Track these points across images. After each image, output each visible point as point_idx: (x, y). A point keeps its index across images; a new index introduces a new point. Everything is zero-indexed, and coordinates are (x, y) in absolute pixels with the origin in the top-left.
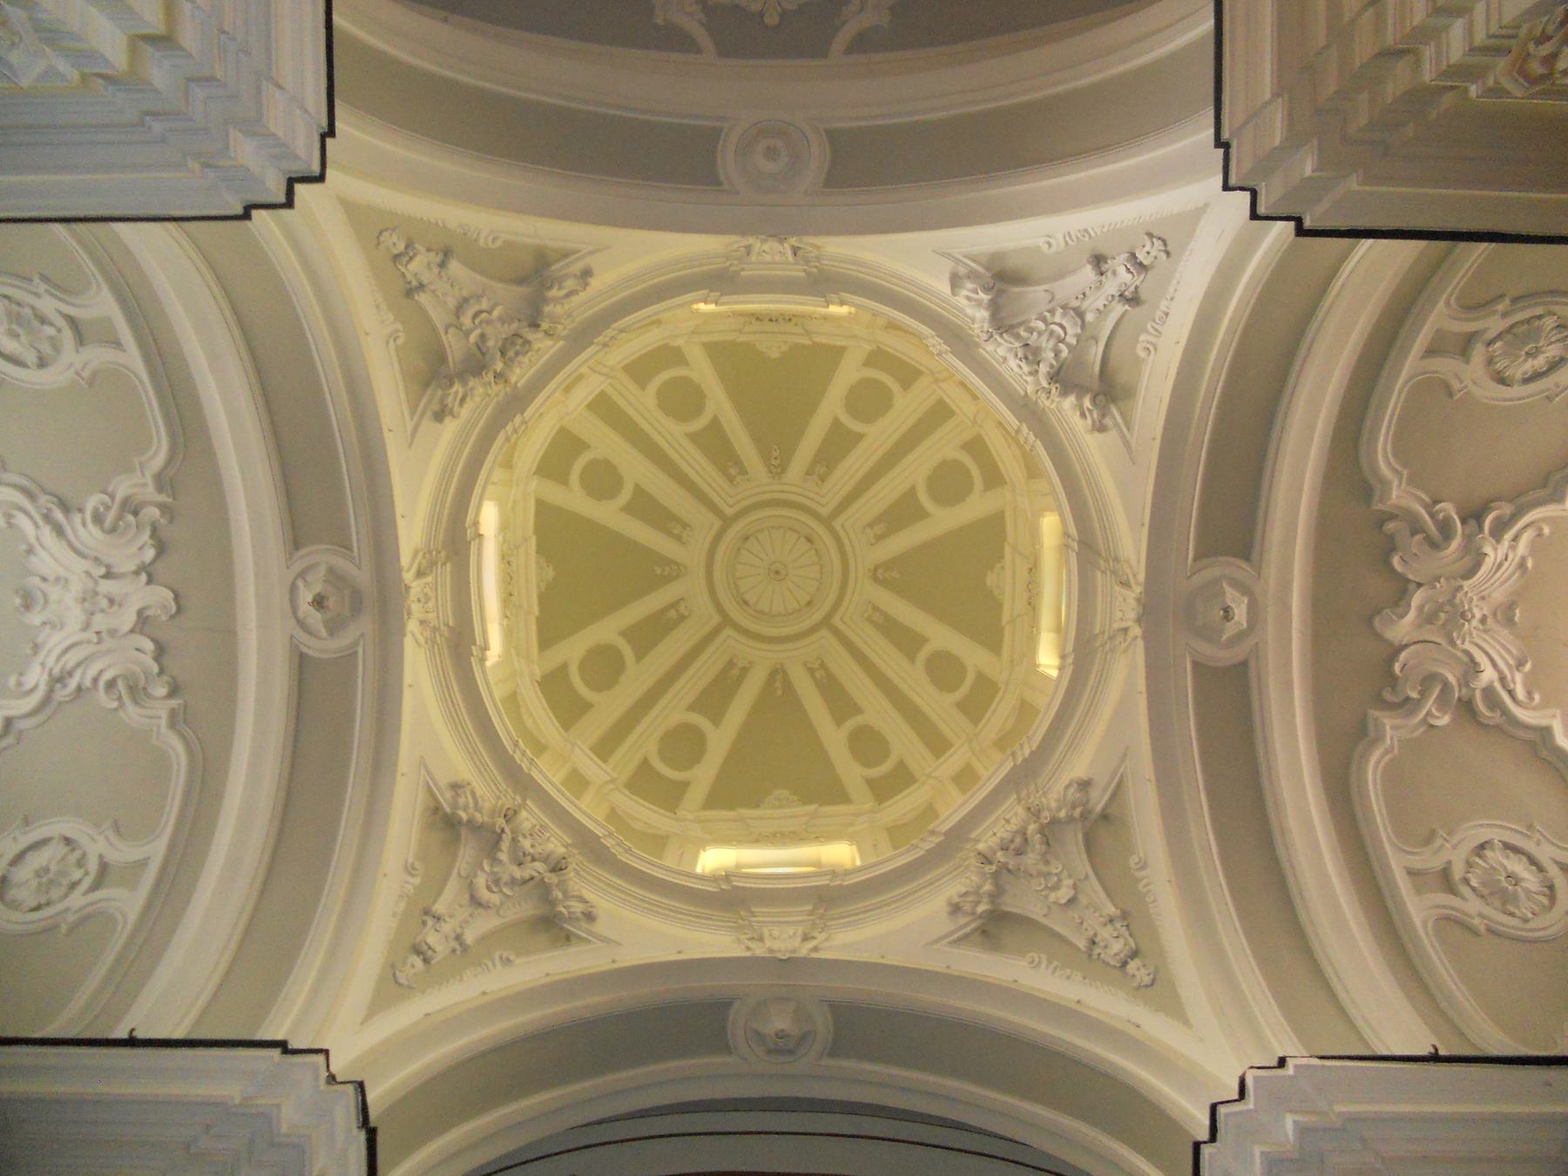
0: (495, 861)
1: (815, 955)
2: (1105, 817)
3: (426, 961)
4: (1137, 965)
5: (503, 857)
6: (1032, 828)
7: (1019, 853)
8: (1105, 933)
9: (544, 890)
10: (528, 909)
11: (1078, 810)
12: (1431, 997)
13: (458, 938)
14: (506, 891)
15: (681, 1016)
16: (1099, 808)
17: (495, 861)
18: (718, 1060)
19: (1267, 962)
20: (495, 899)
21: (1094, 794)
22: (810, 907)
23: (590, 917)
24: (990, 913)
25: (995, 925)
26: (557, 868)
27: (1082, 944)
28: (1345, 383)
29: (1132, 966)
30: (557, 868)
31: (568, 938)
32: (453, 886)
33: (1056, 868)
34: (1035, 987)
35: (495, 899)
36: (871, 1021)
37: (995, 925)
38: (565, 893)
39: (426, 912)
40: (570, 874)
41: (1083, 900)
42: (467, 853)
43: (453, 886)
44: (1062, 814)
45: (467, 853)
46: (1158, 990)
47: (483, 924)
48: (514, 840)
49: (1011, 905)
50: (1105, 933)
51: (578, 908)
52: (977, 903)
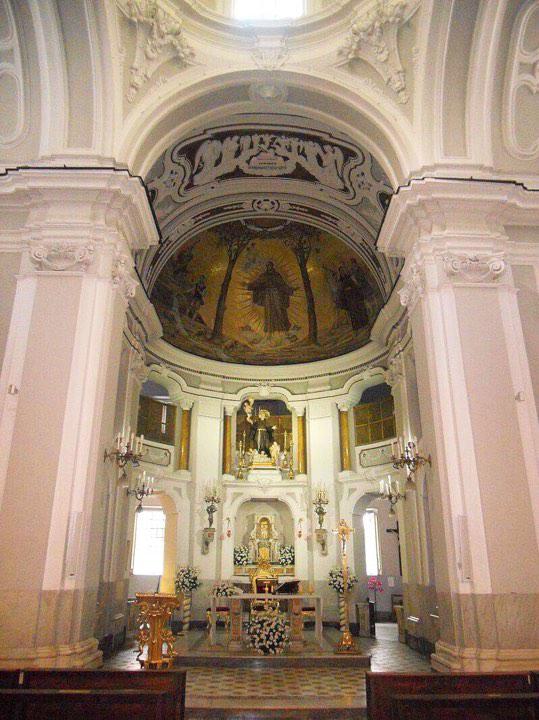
0: (152, 38)
1: (283, 69)
2: (408, 24)
3: (136, 89)
4: (401, 93)
5: (155, 36)
6: (377, 24)
7: (370, 34)
8: (395, 77)
9: (173, 47)
10: (169, 56)
11: (398, 19)
12: (501, 100)
13: (146, 76)
14: (160, 51)
15: (235, 89)
16: (407, 19)
17: (152, 38)
18: (246, 102)
19: (447, 96)
20: (154, 55)
21: (406, 12)
22: (281, 37)
23: (192, 54)
24: (354, 59)
25: (354, 63)
26: (177, 34)
27: (386, 80)
28: (428, 333)
29: (402, 93)
30: (177, 34)
31: (186, 65)
32: (139, 53)
33: (383, 44)
34: (362, 91)
35: (154, 55)
36: (300, 92)
37: (354, 63)
38: (182, 46)
39: (132, 68)
40: (184, 34)
41: (390, 62)
42: (141, 36)
43: (139, 53)
44: (391, 20)
45: (141, 36)
46: (406, 108)
47: (154, 67)
48: (159, 27)
49: (363, 55)
50: (395, 77)
51: (187, 51)
52: (349, 53)
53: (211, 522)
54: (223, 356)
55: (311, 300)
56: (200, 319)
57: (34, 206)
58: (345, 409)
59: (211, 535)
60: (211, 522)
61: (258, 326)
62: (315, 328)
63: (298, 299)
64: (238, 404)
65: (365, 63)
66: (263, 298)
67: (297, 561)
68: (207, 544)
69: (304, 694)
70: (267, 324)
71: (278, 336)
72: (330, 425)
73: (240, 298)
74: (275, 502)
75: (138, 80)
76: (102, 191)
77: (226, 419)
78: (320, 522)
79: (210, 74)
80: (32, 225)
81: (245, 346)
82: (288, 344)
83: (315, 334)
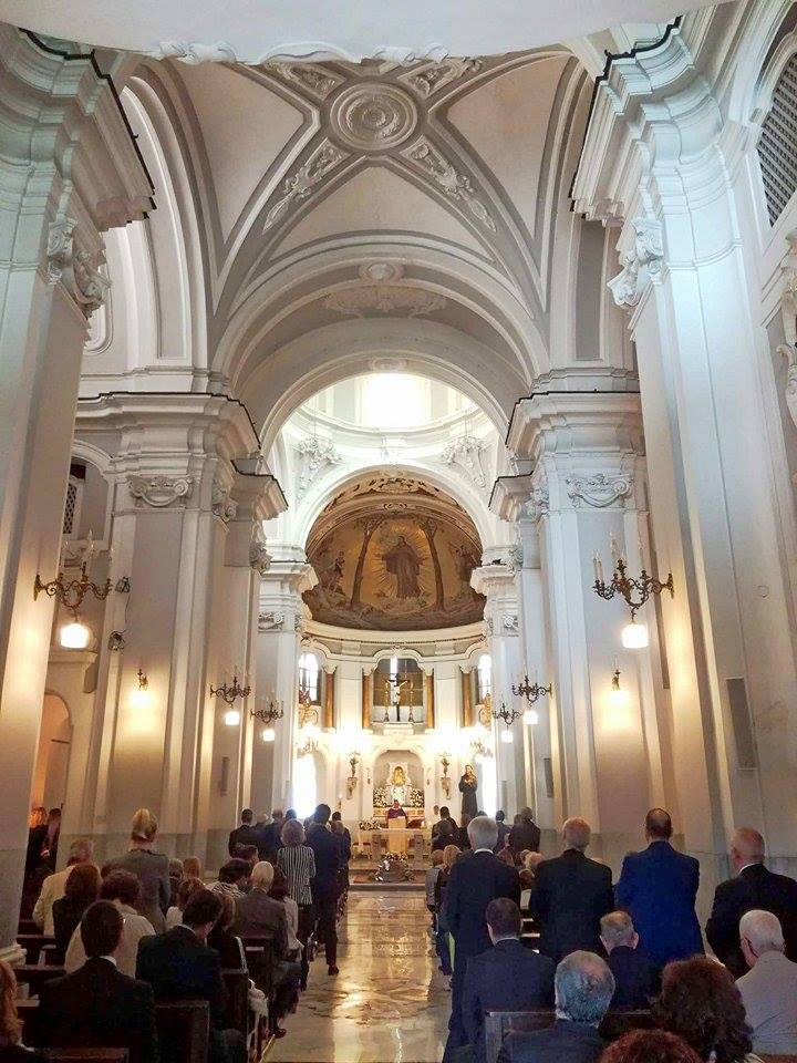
31: (335, 466)
37: (453, 463)
47: (314, 472)
53: (354, 772)
54: (362, 622)
55: (438, 570)
56: (340, 590)
57: (126, 429)
58: (466, 672)
59: (354, 783)
60: (354, 772)
61: (391, 593)
62: (442, 595)
63: (427, 567)
64: (375, 666)
65: (460, 466)
66: (396, 567)
67: (426, 804)
68: (351, 791)
69: (235, 450)
70: (399, 589)
71: (410, 601)
72: (454, 685)
73: (375, 568)
74: (407, 753)
75: (304, 485)
76: (286, 576)
77: (364, 678)
78: (445, 771)
79: (353, 469)
80: (124, 453)
81: (380, 611)
82: (418, 609)
83: (442, 600)
